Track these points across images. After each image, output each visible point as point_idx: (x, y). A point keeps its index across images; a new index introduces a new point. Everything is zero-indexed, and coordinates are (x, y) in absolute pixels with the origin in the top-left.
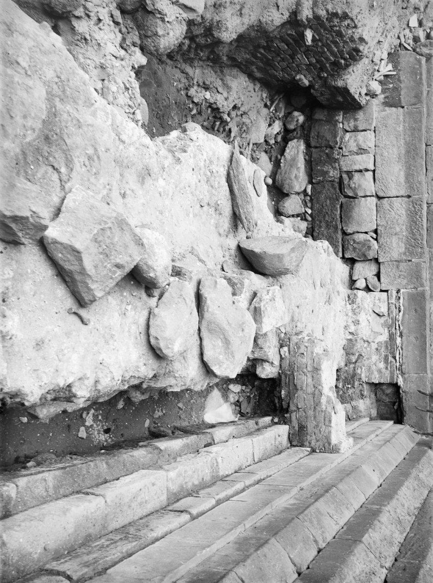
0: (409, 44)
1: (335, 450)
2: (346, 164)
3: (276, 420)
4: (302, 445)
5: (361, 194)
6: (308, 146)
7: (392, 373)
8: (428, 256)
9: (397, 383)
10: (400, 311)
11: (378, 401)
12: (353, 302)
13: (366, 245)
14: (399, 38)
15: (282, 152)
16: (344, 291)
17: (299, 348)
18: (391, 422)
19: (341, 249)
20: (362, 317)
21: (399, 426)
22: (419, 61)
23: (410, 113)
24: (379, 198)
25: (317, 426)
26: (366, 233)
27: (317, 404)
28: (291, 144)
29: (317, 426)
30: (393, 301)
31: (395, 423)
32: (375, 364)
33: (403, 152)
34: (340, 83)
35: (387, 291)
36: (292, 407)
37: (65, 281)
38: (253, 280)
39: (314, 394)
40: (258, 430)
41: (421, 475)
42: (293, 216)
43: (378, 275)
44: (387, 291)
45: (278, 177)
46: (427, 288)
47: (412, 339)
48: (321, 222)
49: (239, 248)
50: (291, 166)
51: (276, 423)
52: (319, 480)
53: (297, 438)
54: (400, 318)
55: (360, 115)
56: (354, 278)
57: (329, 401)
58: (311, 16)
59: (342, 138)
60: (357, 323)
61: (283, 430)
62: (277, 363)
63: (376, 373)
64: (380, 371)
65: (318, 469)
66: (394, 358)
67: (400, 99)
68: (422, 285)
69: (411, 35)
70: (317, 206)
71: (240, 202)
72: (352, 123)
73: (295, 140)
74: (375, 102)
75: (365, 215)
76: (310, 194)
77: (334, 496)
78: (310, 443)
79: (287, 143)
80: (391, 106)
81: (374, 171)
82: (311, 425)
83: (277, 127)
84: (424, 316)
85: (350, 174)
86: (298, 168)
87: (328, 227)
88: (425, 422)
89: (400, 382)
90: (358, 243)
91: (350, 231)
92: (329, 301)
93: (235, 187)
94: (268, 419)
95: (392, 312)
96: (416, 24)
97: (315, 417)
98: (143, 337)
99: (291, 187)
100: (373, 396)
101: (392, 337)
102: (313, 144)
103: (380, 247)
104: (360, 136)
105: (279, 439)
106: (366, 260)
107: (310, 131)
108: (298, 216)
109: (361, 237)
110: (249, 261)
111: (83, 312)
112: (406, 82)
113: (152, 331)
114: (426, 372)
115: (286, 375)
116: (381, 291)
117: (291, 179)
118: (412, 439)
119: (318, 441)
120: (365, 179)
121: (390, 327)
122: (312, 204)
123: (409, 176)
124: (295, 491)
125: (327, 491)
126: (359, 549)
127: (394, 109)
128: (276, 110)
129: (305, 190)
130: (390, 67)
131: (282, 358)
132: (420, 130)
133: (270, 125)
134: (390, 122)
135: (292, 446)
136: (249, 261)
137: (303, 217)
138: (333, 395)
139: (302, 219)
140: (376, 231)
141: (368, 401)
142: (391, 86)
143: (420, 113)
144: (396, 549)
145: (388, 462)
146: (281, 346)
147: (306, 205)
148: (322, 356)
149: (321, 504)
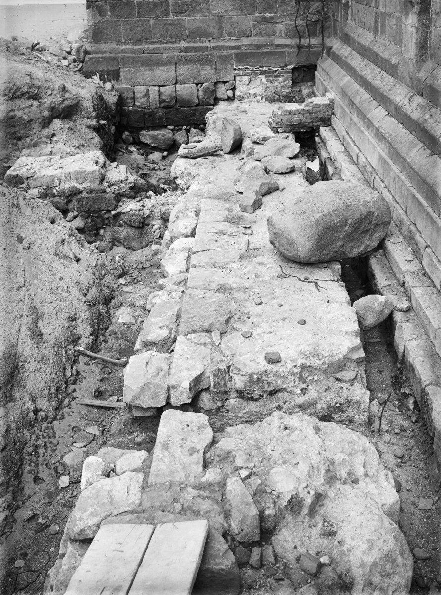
0: (78, 65)
1: (332, 101)
2: (155, 105)
3: (317, 134)
4: (331, 119)
5: (174, 94)
6: (143, 129)
7: (286, 73)
8: (213, 51)
9: (292, 69)
10: (247, 68)
11: (302, 81)
12: (243, 98)
13: (206, 91)
14: (76, 72)
15: (147, 145)
16: (236, 104)
17: (279, 122)
18: (316, 72)
19: (209, 107)
20: (252, 92)
21: (318, 67)
22: (90, 58)
23: (124, 64)
24: (176, 83)
25: (320, 111)
26: (198, 90)
27: (308, 111)
28: (142, 139)
29: (320, 111)
30: (241, 72)
31: (316, 70)
32: (280, 83)
33: (148, 68)
34: (113, 107)
35: (235, 77)
36: (310, 125)
37: (271, 193)
38: (247, 144)
39: (303, 114)
40: (323, 142)
41: (346, 55)
42: (188, 138)
43: (225, 82)
44: (235, 77)
45: (163, 147)
46: (233, 51)
47: (264, 60)
48: (191, 120)
49: (229, 153)
50: (157, 139)
51: (319, 134)
52: (347, 106)
53: (327, 122)
54: (252, 68)
55: (125, 95)
56: (226, 97)
57: (307, 105)
58: (96, 120)
59: (139, 107)
60: (255, 95)
61: (323, 130)
62: (287, 134)
63: (286, 83)
64: (284, 80)
65: (342, 107)
66: (276, 71)
67: (114, 71)
68: (231, 54)
69: (73, 64)
70: (181, 122)
71: (207, 152)
72: (130, 101)
73: (140, 137)
74: (116, 86)
75: (187, 90)
76: (173, 127)
77: (354, 97)
78: (329, 115)
79: (142, 142)
80: (118, 76)
81: (159, 86)
82: (320, 115)
83: (133, 149)
84: (250, 53)
85: (162, 101)
86: (158, 135)
87: (194, 115)
88: (315, 51)
89: (291, 67)
90: (205, 96)
91: (197, 101)
92: (245, 111)
93: (200, 154)
94: (317, 139)
95: (248, 73)
96: (67, 61)
97: (315, 113)
98: (287, 175)
99: (170, 139)
100: (300, 84)
101: (263, 73)
102: (142, 125)
103: (207, 82)
104: (138, 95)
105: (327, 130)
106: (214, 91)
107: (135, 128)
108: (187, 135)
109: (201, 93)
110: (236, 148)
111: (281, 189)
112: (104, 67)
113: (284, 171)
114: (284, 51)
115: (293, 129)
116: (235, 80)
117: (164, 140)
118: (326, 59)
119: (328, 111)
120: (165, 92)
121: (257, 75)
122: (180, 125)
123: (163, 64)
124: (351, 115)
125: (351, 100)
126: (373, 83)
127: (121, 74)
128: (123, 149)
129: (171, 130)
130: (95, 77)
131: (284, 132)
132: (134, 58)
133: (132, 152)
134: (129, 76)
135: (331, 125)
136: (236, 148)
137: (188, 131)
138: (303, 104)
139: (189, 132)
140: (197, 84)
141: (303, 88)
142: (106, 76)
143: (123, 57)
144: (376, 67)
145: (339, 73)
146: (278, 132)
147: (181, 130)
148: (283, 110)
149: (356, 102)
